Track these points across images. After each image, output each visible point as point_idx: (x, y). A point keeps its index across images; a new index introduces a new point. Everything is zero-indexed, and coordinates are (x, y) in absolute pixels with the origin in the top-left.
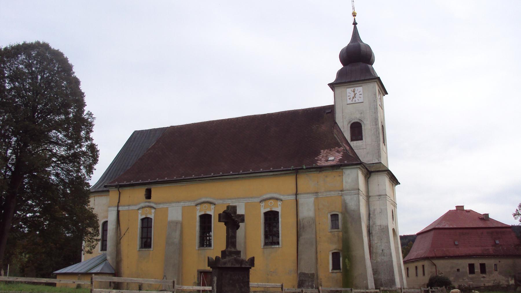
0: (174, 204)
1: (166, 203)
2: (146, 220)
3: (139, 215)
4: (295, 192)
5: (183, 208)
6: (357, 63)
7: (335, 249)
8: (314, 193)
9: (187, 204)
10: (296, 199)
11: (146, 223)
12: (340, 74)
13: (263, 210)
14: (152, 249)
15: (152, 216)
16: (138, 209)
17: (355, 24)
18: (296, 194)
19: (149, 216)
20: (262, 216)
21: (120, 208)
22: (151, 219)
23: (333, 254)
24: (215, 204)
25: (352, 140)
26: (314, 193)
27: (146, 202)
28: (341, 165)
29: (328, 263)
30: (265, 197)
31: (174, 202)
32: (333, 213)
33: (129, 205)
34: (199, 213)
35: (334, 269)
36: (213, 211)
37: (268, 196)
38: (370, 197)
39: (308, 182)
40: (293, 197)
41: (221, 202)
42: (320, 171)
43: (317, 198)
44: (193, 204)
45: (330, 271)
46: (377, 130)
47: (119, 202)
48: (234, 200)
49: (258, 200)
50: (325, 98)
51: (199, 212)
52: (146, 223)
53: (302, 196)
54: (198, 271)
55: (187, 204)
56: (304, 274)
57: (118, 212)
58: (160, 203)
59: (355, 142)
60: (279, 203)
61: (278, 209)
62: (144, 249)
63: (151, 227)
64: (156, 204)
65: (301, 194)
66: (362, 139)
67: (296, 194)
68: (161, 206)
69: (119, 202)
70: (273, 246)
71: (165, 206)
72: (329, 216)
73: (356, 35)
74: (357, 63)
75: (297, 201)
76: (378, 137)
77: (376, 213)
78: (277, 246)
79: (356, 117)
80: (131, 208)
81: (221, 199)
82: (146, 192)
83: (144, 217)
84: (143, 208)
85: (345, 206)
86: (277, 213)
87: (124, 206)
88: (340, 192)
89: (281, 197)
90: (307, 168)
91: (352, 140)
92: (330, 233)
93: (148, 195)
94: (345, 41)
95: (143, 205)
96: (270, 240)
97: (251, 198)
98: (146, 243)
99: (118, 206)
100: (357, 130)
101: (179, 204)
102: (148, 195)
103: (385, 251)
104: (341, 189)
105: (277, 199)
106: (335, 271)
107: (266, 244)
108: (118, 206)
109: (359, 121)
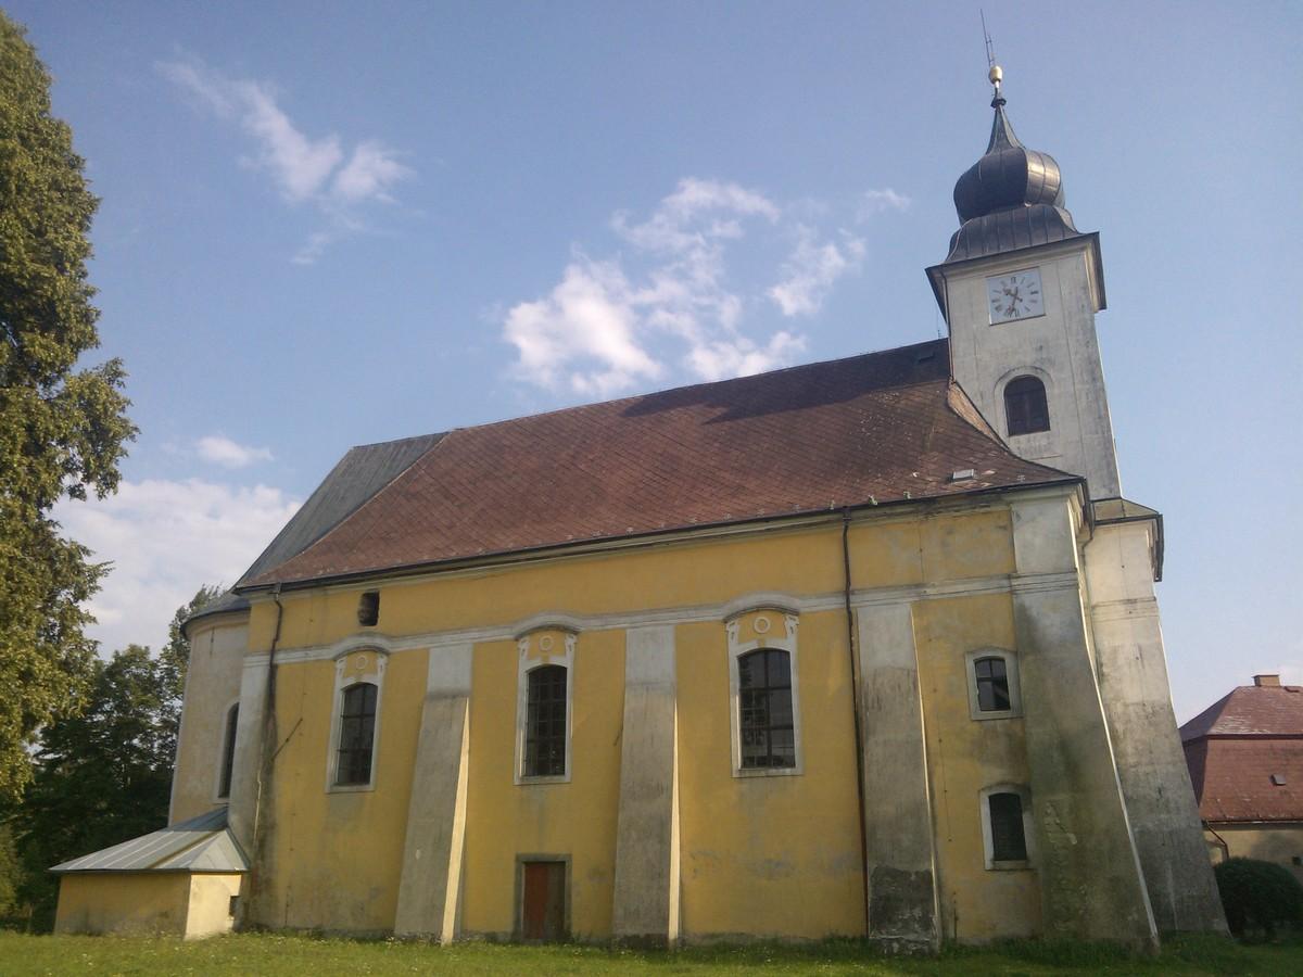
0: (446, 638)
1: (415, 635)
2: (359, 692)
3: (523, 659)
4: (840, 583)
5: (478, 648)
6: (1004, 211)
7: (1002, 784)
8: (909, 587)
9: (489, 635)
10: (848, 607)
11: (360, 700)
12: (958, 242)
13: (737, 649)
14: (370, 787)
15: (377, 680)
16: (335, 660)
17: (998, 103)
18: (847, 592)
19: (366, 679)
20: (734, 665)
21: (280, 658)
22: (375, 687)
23: (994, 800)
24: (575, 632)
25: (1012, 433)
26: (909, 587)
27: (361, 635)
28: (1005, 490)
29: (979, 835)
30: (741, 603)
31: (444, 631)
32: (984, 654)
33: (307, 648)
34: (526, 664)
35: (998, 857)
36: (570, 654)
37: (753, 600)
38: (1094, 607)
39: (883, 549)
40: (836, 603)
41: (595, 624)
42: (928, 514)
43: (921, 607)
44: (507, 635)
45: (988, 865)
46: (1097, 400)
47: (277, 639)
48: (638, 618)
49: (720, 614)
50: (912, 321)
51: (527, 660)
52: (360, 700)
53: (868, 597)
54: (518, 858)
55: (489, 635)
56: (895, 874)
57: (273, 669)
58: (403, 637)
59: (1023, 438)
60: (791, 623)
61: (788, 644)
62: (346, 788)
63: (373, 715)
64: (390, 637)
65: (863, 591)
66: (1045, 427)
67: (847, 592)
68: (406, 645)
69: (277, 639)
70: (773, 771)
71: (420, 644)
72: (970, 665)
73: (998, 133)
74: (1004, 211)
75: (850, 613)
76: (956, 598)
77: (1121, 660)
78: (788, 771)
79: (1022, 362)
80: (313, 655)
81: (596, 616)
82: (362, 603)
83: (351, 681)
84: (350, 652)
85: (1023, 622)
86: (564, 670)
87: (293, 649)
88: (1005, 582)
89: (796, 603)
90: (882, 505)
91: (1012, 433)
92: (976, 726)
93: (370, 616)
94: (972, 150)
95: (350, 643)
96: (762, 752)
97: (696, 608)
98: (356, 765)
99: (273, 652)
100: (1027, 401)
101: (462, 636)
102: (370, 616)
103: (1169, 794)
104: (1006, 571)
105: (782, 610)
106: (1006, 864)
107: (748, 761)
108: (273, 652)
109: (1029, 372)
